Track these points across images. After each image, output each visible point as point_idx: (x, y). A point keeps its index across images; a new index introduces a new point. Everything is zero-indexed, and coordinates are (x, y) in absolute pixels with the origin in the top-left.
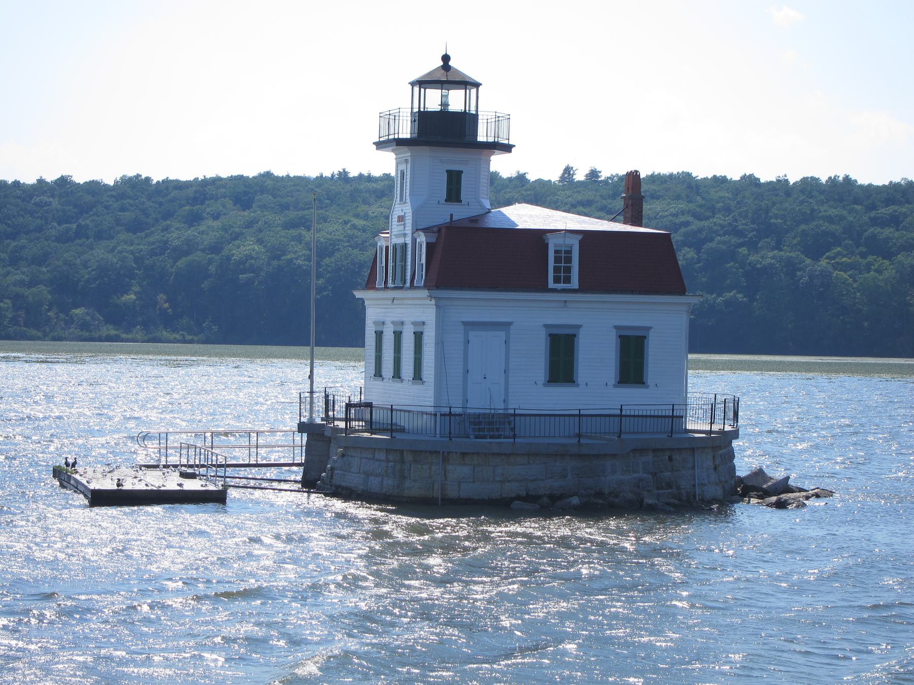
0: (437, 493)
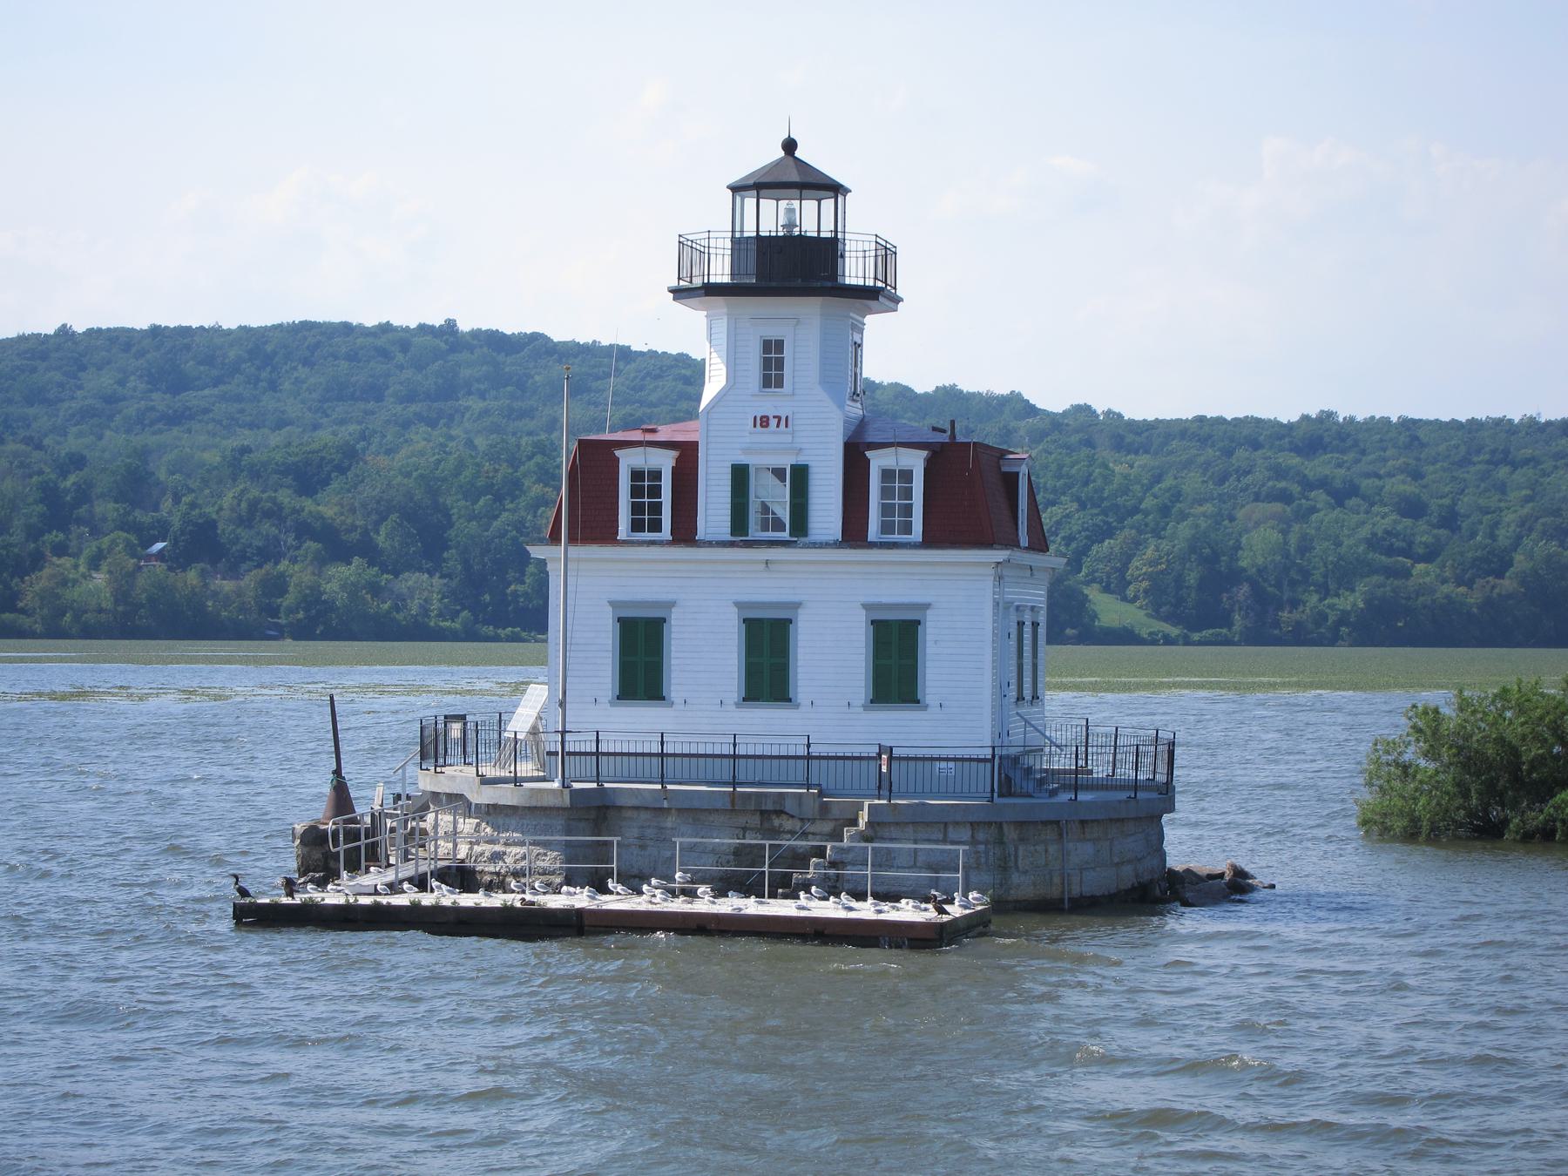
0: (1055, 893)
